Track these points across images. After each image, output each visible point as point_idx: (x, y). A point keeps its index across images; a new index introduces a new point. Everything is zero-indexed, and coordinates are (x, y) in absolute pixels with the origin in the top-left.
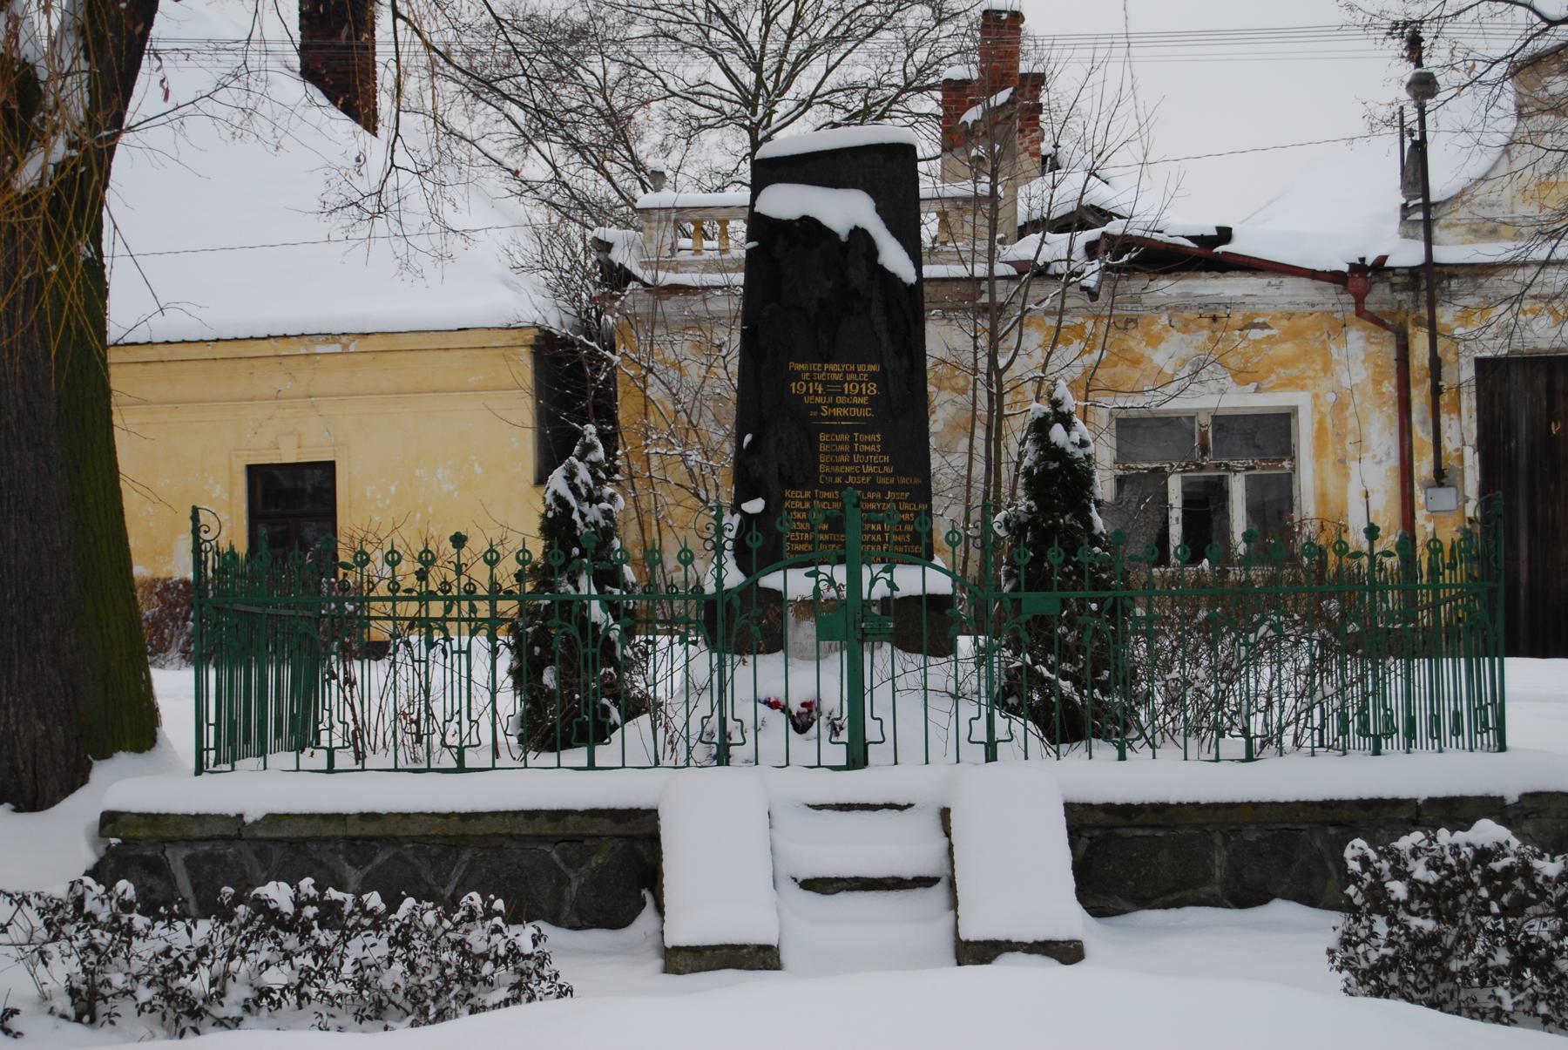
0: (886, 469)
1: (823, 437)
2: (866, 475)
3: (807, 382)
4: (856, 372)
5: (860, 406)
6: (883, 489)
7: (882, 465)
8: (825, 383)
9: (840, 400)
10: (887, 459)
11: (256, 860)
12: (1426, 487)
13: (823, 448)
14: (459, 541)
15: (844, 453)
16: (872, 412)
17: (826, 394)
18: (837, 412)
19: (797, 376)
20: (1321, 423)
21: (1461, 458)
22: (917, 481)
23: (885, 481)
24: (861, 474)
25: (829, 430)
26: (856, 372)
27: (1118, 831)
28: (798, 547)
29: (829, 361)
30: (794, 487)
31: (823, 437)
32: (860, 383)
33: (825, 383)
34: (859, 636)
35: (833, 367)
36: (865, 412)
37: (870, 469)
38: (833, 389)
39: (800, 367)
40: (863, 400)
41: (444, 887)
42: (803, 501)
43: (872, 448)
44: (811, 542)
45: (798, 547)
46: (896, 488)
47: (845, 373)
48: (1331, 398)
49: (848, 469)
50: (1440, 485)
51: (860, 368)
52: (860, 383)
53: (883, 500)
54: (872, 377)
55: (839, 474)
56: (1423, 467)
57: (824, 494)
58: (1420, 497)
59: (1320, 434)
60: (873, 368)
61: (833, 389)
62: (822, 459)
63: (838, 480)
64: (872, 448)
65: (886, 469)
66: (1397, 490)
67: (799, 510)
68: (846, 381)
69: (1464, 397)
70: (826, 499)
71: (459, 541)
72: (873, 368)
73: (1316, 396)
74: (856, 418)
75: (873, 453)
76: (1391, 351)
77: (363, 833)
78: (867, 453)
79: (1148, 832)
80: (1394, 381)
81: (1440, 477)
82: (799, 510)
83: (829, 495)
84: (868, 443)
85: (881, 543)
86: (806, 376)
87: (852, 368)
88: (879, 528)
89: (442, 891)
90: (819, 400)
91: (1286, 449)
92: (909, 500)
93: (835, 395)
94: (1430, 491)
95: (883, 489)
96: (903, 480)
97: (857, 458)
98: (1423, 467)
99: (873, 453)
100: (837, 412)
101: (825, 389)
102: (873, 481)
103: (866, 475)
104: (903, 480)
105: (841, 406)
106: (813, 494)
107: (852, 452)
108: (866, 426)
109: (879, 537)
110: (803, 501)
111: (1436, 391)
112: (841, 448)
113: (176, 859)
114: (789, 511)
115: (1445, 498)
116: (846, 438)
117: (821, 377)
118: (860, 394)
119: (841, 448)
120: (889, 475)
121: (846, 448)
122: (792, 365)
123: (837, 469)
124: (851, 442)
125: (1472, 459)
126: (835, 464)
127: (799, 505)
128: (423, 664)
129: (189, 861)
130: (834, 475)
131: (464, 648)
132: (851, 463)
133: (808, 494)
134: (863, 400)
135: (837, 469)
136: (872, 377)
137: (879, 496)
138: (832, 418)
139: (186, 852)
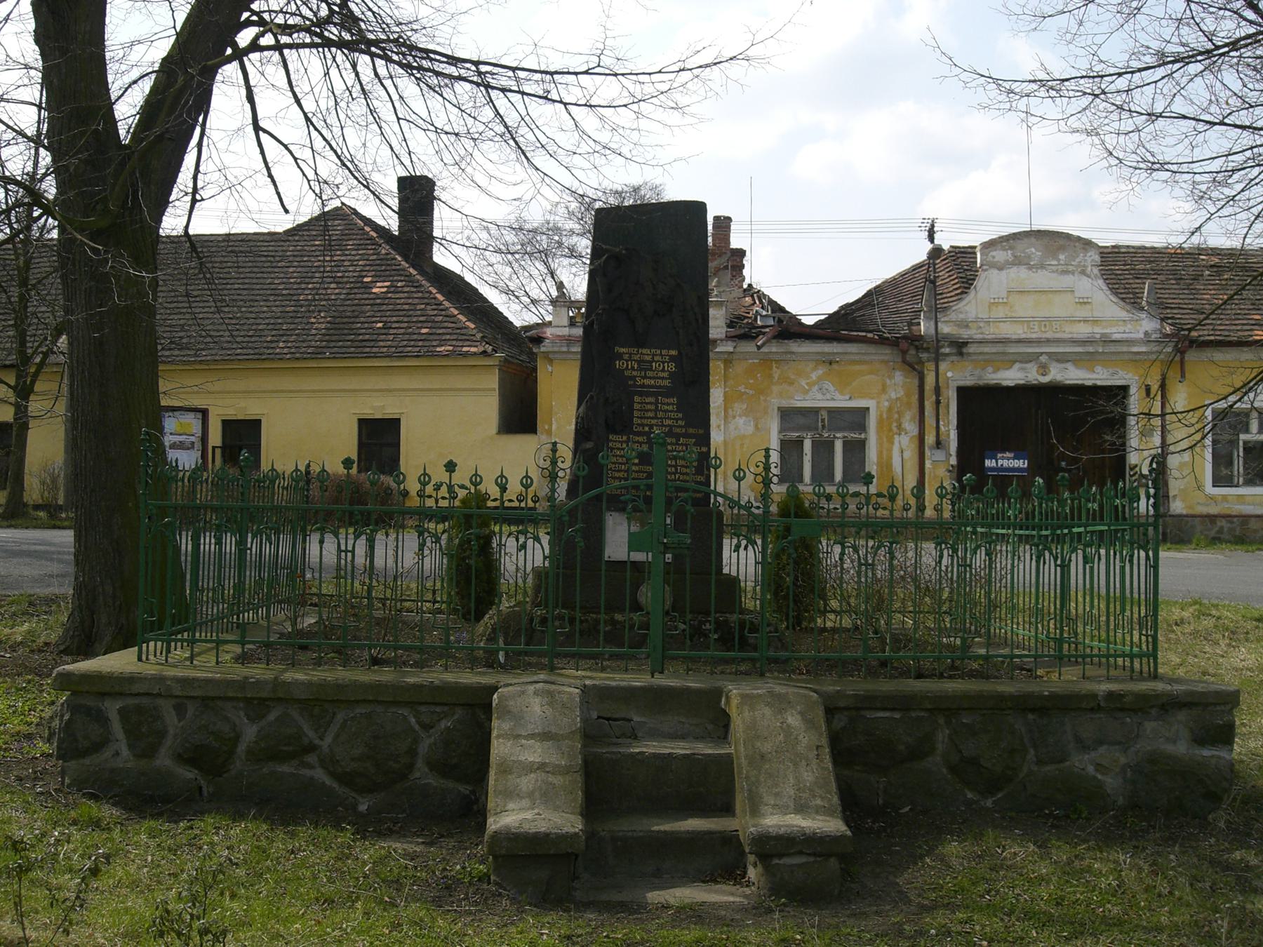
0: (680, 422)
1: (637, 399)
2: (666, 426)
3: (627, 361)
4: (661, 355)
5: (663, 378)
6: (678, 436)
7: (677, 420)
8: (639, 362)
9: (650, 374)
10: (680, 415)
11: (174, 713)
12: (931, 448)
13: (636, 406)
14: (451, 467)
15: (650, 410)
16: (672, 383)
17: (640, 369)
18: (647, 382)
19: (620, 356)
20: (881, 416)
21: (949, 435)
22: (701, 432)
23: (678, 430)
24: (663, 425)
25: (641, 394)
26: (661, 355)
27: (863, 713)
28: (617, 475)
29: (642, 347)
30: (616, 433)
31: (637, 399)
32: (663, 363)
33: (639, 362)
34: (662, 549)
35: (644, 351)
36: (667, 383)
37: (668, 422)
38: (644, 366)
39: (623, 350)
40: (665, 375)
41: (322, 739)
42: (622, 442)
43: (670, 408)
44: (627, 471)
45: (617, 475)
46: (686, 435)
47: (654, 355)
48: (886, 404)
49: (654, 422)
50: (938, 448)
51: (664, 352)
52: (663, 363)
53: (677, 444)
54: (672, 358)
55: (647, 425)
56: (930, 439)
57: (637, 438)
58: (928, 453)
59: (880, 422)
60: (673, 352)
61: (644, 366)
62: (636, 414)
63: (647, 429)
64: (670, 408)
65: (680, 422)
66: (917, 450)
67: (618, 449)
68: (653, 361)
69: (951, 406)
70: (638, 442)
71: (451, 467)
72: (673, 352)
73: (878, 403)
74: (660, 387)
75: (671, 411)
76: (916, 382)
77: (258, 695)
78: (666, 411)
79: (887, 714)
80: (917, 396)
81: (938, 444)
82: (618, 449)
83: (641, 439)
84: (668, 404)
85: (675, 474)
86: (626, 357)
87: (659, 352)
88: (674, 463)
89: (321, 743)
90: (635, 373)
91: (862, 427)
92: (695, 444)
93: (646, 370)
94: (933, 452)
95: (678, 436)
96: (691, 431)
97: (660, 414)
98: (930, 439)
99: (671, 411)
100: (647, 382)
101: (639, 366)
102: (670, 431)
103: (666, 426)
104: (691, 431)
105: (650, 378)
106: (628, 438)
107: (656, 410)
108: (668, 393)
109: (673, 469)
110: (622, 442)
111: (938, 402)
112: (649, 407)
113: (112, 708)
114: (612, 449)
115: (939, 455)
116: (652, 399)
117: (636, 357)
118: (663, 370)
119: (649, 407)
120: (680, 426)
121: (653, 407)
122: (617, 349)
123: (645, 421)
124: (656, 403)
125: (953, 435)
126: (645, 418)
127: (619, 445)
128: (349, 554)
129: (121, 712)
130: (643, 425)
131: (350, 548)
132: (655, 417)
133: (625, 438)
134: (665, 375)
135: (645, 421)
136: (672, 358)
137: (674, 440)
138: (643, 386)
139: (118, 704)
